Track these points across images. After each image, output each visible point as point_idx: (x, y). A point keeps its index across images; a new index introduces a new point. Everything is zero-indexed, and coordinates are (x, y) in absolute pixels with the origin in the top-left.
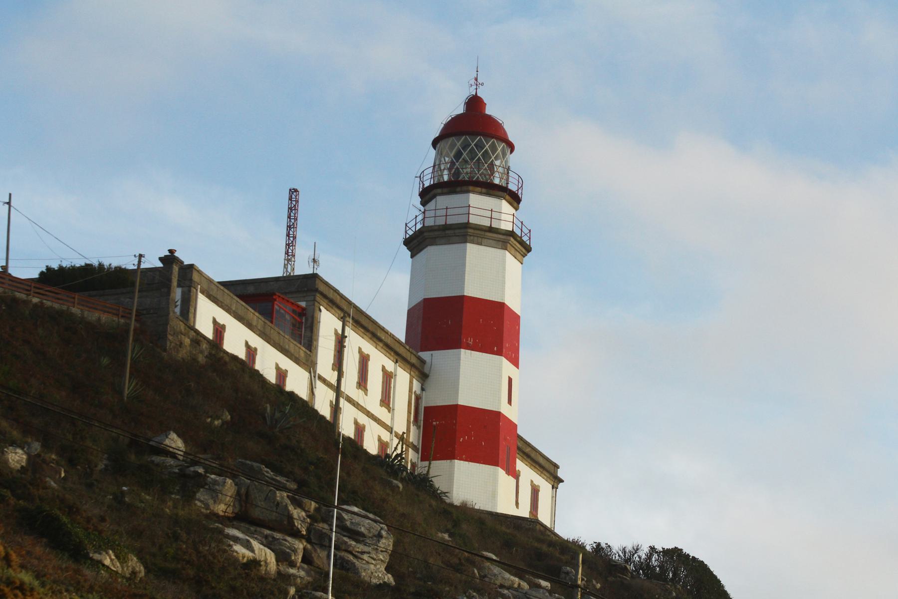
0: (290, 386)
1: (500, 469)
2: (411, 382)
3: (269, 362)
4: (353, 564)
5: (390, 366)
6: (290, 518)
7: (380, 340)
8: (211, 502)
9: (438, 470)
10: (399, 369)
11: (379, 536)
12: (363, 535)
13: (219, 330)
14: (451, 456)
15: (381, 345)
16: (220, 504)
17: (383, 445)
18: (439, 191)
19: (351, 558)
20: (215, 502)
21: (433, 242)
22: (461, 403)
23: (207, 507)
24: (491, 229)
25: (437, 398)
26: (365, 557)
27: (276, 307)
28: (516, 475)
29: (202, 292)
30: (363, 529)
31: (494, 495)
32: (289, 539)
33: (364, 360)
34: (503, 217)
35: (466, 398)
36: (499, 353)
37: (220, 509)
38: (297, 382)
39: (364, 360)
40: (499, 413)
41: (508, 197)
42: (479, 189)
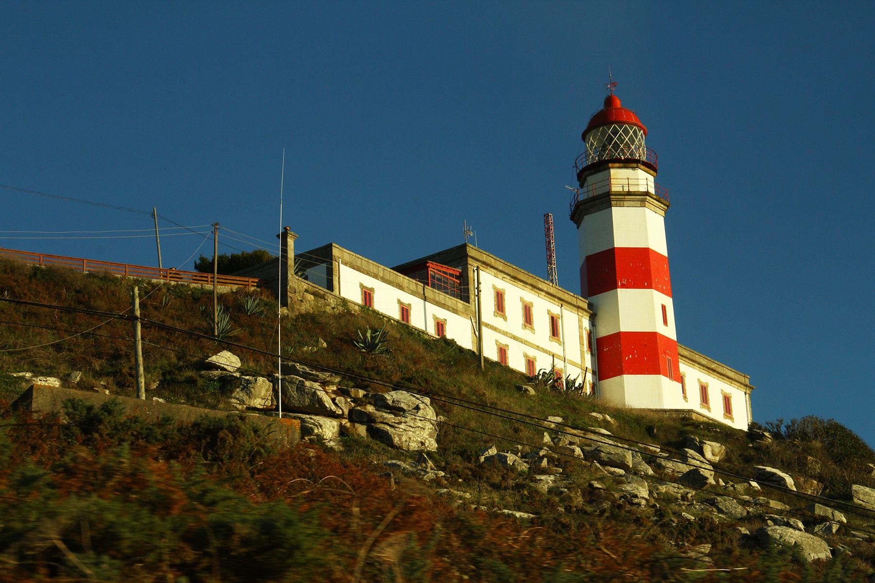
0: (417, 321)
1: (661, 377)
2: (580, 321)
3: (425, 315)
4: (387, 433)
5: (555, 309)
6: (320, 401)
7: (542, 290)
8: (245, 398)
9: (610, 384)
10: (564, 310)
11: (417, 408)
12: (404, 410)
13: (368, 295)
14: (620, 373)
15: (544, 294)
16: (255, 398)
17: (530, 363)
18: (588, 172)
19: (388, 428)
20: (250, 397)
21: (588, 212)
22: (623, 329)
23: (242, 402)
24: (629, 193)
25: (604, 331)
26: (403, 426)
27: (430, 272)
28: (680, 379)
29: (346, 264)
30: (402, 405)
31: (660, 397)
32: (313, 417)
33: (500, 297)
34: (640, 182)
35: (626, 326)
36: (650, 287)
37: (258, 403)
38: (460, 332)
39: (500, 297)
40: (655, 333)
41: (642, 167)
42: (617, 165)
